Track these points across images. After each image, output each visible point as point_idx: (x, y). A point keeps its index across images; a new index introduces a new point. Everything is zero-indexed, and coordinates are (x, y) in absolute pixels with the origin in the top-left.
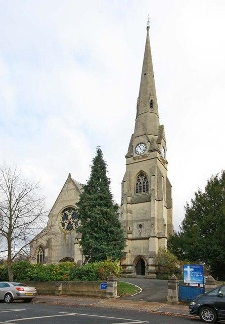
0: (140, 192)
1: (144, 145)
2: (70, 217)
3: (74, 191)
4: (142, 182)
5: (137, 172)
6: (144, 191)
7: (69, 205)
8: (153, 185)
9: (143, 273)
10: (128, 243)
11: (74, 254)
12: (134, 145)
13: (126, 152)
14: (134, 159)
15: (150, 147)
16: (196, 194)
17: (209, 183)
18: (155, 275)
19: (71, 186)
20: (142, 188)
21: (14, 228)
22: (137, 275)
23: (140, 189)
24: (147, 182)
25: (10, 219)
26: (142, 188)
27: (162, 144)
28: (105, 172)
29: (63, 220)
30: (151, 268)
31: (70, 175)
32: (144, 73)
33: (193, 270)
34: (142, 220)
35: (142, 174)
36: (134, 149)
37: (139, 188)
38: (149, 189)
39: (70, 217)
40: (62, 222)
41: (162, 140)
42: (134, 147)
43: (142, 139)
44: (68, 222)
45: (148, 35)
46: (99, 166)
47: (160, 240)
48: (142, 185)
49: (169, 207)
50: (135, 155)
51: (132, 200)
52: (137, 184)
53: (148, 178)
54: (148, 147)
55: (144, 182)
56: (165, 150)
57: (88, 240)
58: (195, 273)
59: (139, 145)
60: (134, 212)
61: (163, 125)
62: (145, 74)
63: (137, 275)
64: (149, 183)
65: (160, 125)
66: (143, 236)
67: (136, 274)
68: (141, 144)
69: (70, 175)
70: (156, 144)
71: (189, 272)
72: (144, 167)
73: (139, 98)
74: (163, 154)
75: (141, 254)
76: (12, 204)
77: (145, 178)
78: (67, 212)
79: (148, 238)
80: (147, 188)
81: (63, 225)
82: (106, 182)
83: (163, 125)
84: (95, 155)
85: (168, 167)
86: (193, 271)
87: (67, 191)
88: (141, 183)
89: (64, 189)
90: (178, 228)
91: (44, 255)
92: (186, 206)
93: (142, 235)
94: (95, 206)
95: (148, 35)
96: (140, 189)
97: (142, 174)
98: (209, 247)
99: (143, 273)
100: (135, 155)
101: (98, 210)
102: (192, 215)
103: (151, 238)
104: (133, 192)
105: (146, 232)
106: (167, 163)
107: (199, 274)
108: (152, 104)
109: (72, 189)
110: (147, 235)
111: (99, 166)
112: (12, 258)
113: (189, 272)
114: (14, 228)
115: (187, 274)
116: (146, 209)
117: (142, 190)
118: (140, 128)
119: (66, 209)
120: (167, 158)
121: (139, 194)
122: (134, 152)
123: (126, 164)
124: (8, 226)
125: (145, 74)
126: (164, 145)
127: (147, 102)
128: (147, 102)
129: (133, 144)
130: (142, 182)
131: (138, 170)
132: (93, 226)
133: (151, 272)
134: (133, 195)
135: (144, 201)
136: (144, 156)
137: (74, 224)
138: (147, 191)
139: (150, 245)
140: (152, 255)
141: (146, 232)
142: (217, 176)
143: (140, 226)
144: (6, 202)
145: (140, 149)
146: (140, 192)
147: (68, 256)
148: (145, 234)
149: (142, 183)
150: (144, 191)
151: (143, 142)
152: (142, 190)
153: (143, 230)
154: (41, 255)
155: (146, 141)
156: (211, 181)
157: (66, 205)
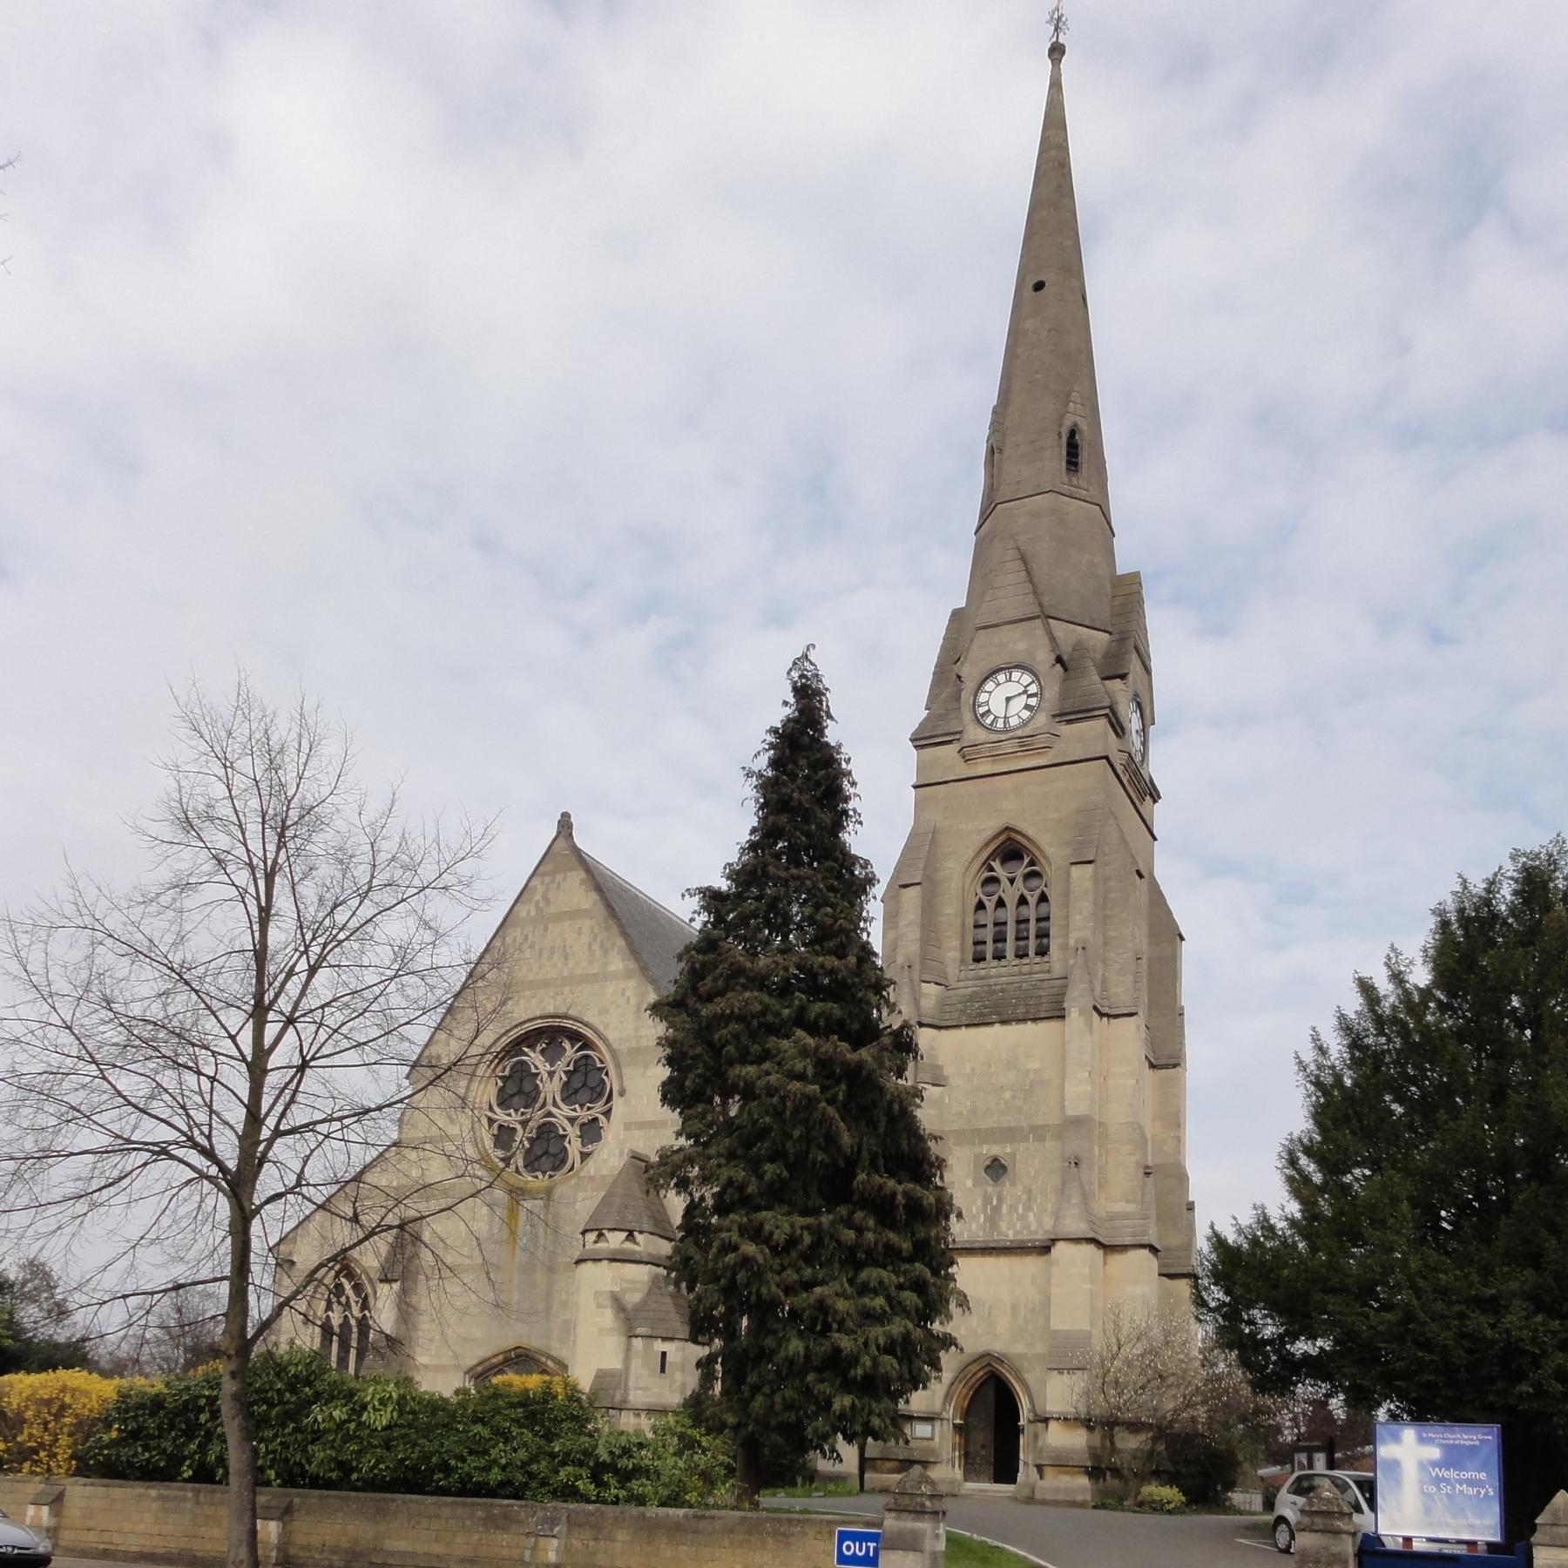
0: (999, 956)
1: (1027, 679)
2: (551, 1088)
3: (587, 924)
4: (1010, 895)
5: (989, 834)
6: (1021, 954)
7: (551, 1010)
8: (1075, 923)
9: (1005, 1470)
10: (968, 1274)
11: (415, 1327)
12: (969, 671)
13: (917, 714)
14: (965, 756)
15: (1064, 695)
16: (1366, 988)
17: (1444, 925)
18: (1084, 1481)
19: (574, 893)
20: (1011, 935)
21: (277, 1133)
22: (968, 1476)
23: (1000, 939)
24: (1043, 898)
25: (257, 1069)
26: (1011, 935)
27: (1130, 677)
28: (839, 819)
29: (504, 1101)
30: (1058, 1437)
31: (565, 824)
32: (1031, 282)
33: (1434, 1453)
34: (1009, 1134)
35: (1010, 848)
36: (966, 696)
37: (988, 934)
38: (1055, 944)
39: (551, 1088)
40: (501, 1116)
41: (1134, 656)
42: (969, 686)
43: (1018, 642)
44: (537, 1118)
45: (1056, 84)
46: (802, 777)
47: (1117, 1260)
48: (1009, 914)
49: (1165, 1058)
50: (974, 734)
51: (942, 1004)
52: (980, 906)
53: (1051, 871)
54: (1052, 692)
55: (1023, 901)
56: (1147, 720)
57: (735, 1248)
58: (1452, 1474)
59: (1001, 677)
60: (954, 1081)
61: (1137, 574)
62: (1039, 286)
63: (968, 1476)
64: (1055, 908)
65: (1119, 573)
66: (1009, 1232)
67: (958, 1473)
68: (1009, 668)
69: (565, 824)
70: (1097, 678)
71: (1410, 1472)
72: (1037, 806)
73: (999, 413)
74: (1136, 740)
75: (998, 1347)
76: (271, 968)
77: (1027, 876)
78: (535, 1058)
79: (1045, 1249)
80: (1043, 935)
81: (504, 1136)
82: (845, 881)
83: (1137, 574)
84: (777, 709)
85: (1160, 814)
86: (1434, 1464)
87: (543, 920)
88: (1001, 903)
89: (522, 911)
90: (1242, 1180)
91: (364, 1325)
92: (1309, 1055)
93: (1003, 1225)
94: (780, 1030)
95: (1056, 84)
96: (1000, 939)
97: (1010, 848)
98: (1479, 1321)
99: (1005, 1470)
100: (974, 734)
101: (804, 1052)
102: (1372, 1102)
103: (1060, 1245)
104: (952, 951)
105: (1028, 1208)
106: (1155, 796)
107: (1471, 1483)
108: (1077, 451)
109: (576, 914)
110: (1036, 1226)
111: (802, 777)
112: (250, 1333)
113: (1410, 1472)
114: (277, 1133)
115: (1398, 1483)
116: (1034, 1065)
117: (1010, 947)
118: (1010, 576)
119: (529, 1039)
120: (1158, 769)
121: (991, 967)
122: (967, 716)
123: (914, 780)
124: (238, 1116)
125: (1039, 286)
126: (1141, 689)
127: (1048, 429)
128: (1048, 429)
129: (965, 670)
130: (1010, 895)
131: (987, 826)
132: (762, 1148)
133: (1062, 1464)
134: (952, 971)
135: (965, 1020)
136: (1026, 743)
137: (573, 1132)
138: (1042, 951)
139: (1055, 1290)
140: (1065, 1357)
141: (1028, 1208)
142: (1492, 885)
143: (996, 1169)
144: (237, 961)
145: (1007, 700)
146: (999, 956)
147: (524, 1342)
148: (1023, 1217)
149: (1011, 902)
150: (1021, 954)
151: (1020, 659)
152: (1010, 947)
153: (1011, 1191)
154: (345, 1324)
155: (1044, 657)
156: (1461, 911)
157: (527, 1010)
